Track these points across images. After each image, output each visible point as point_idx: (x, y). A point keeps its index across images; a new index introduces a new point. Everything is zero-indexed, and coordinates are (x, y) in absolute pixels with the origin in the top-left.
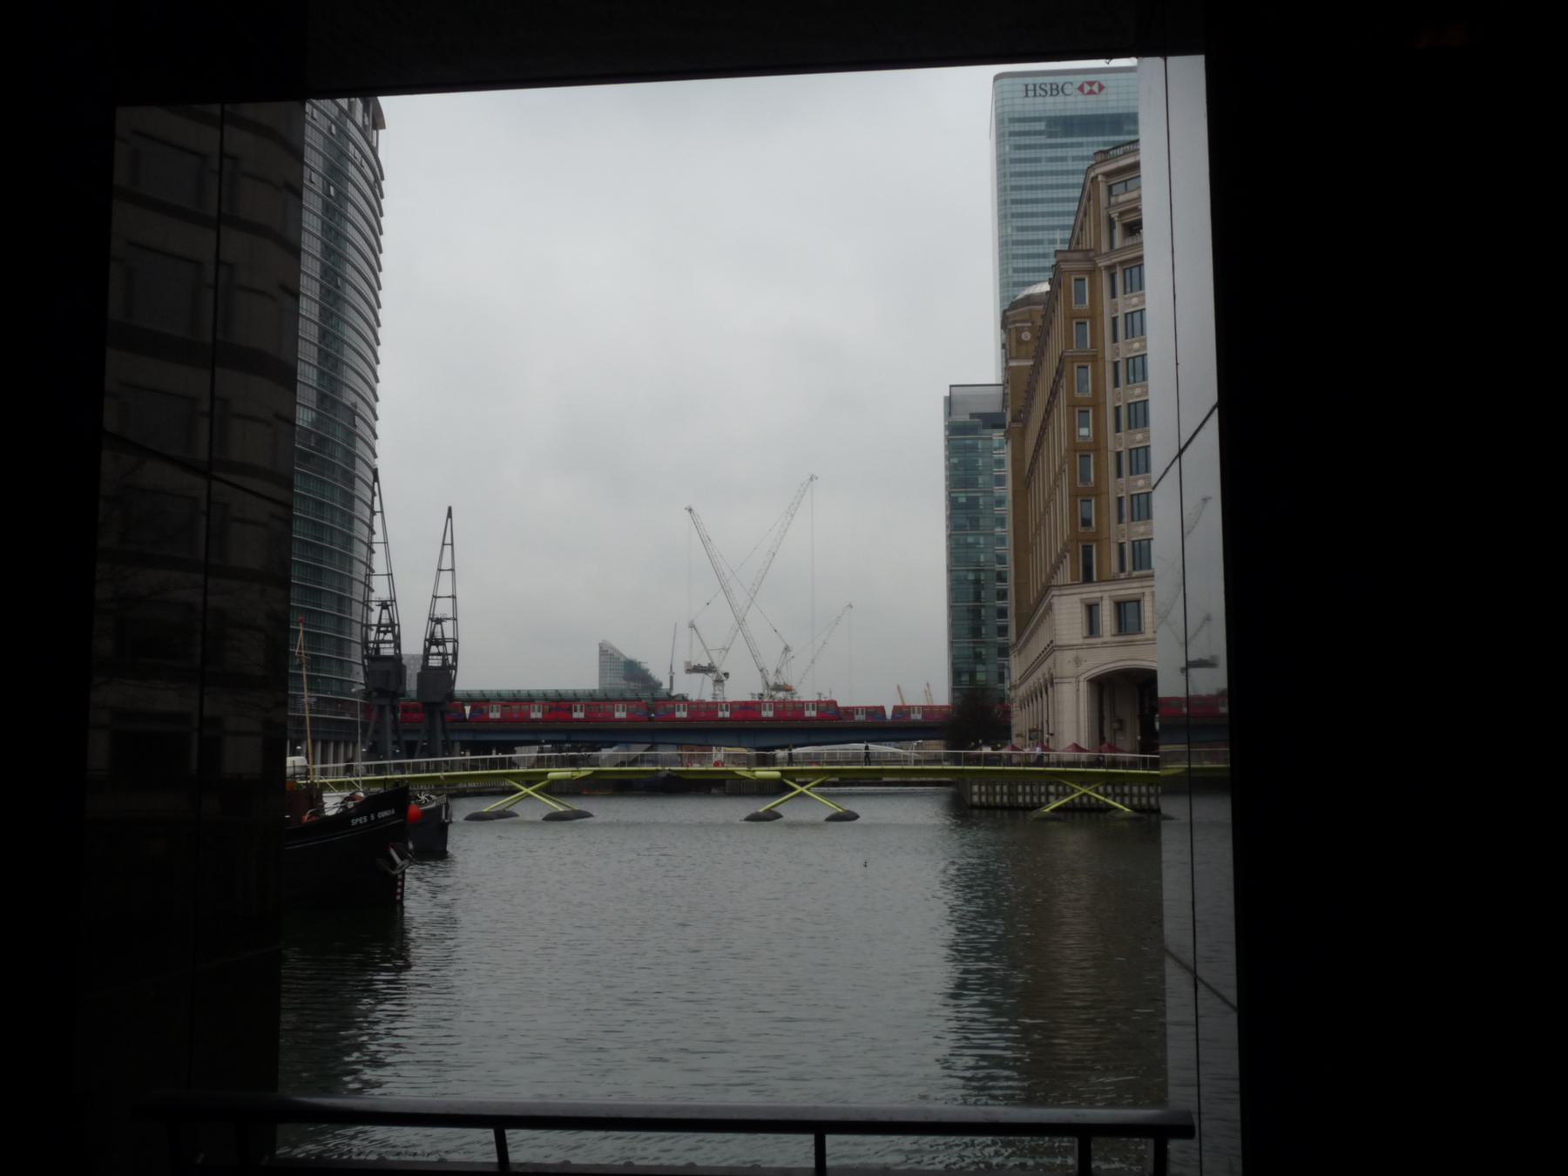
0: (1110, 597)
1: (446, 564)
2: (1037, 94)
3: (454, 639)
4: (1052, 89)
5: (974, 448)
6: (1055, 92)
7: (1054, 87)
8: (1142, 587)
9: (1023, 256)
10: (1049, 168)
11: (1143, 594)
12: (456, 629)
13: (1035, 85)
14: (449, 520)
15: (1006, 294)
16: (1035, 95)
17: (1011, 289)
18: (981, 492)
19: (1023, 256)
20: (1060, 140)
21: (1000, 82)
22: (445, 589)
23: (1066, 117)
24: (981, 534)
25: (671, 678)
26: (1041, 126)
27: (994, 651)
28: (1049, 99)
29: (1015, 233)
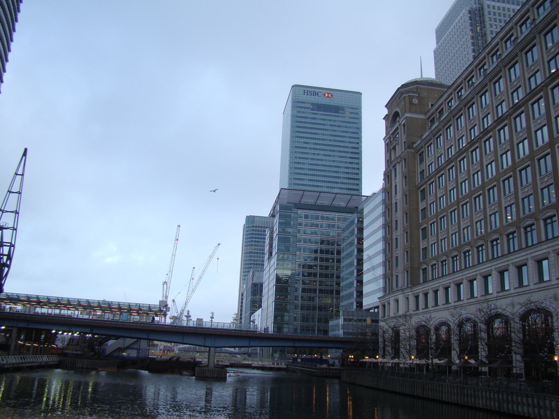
1: (20, 172)
2: (308, 94)
3: (11, 243)
5: (290, 217)
6: (315, 95)
7: (315, 93)
9: (299, 153)
12: (14, 236)
13: (307, 91)
14: (24, 157)
16: (307, 95)
18: (291, 235)
19: (299, 153)
20: (315, 112)
21: (294, 88)
22: (11, 206)
24: (290, 254)
25: (204, 271)
26: (309, 106)
27: (293, 307)
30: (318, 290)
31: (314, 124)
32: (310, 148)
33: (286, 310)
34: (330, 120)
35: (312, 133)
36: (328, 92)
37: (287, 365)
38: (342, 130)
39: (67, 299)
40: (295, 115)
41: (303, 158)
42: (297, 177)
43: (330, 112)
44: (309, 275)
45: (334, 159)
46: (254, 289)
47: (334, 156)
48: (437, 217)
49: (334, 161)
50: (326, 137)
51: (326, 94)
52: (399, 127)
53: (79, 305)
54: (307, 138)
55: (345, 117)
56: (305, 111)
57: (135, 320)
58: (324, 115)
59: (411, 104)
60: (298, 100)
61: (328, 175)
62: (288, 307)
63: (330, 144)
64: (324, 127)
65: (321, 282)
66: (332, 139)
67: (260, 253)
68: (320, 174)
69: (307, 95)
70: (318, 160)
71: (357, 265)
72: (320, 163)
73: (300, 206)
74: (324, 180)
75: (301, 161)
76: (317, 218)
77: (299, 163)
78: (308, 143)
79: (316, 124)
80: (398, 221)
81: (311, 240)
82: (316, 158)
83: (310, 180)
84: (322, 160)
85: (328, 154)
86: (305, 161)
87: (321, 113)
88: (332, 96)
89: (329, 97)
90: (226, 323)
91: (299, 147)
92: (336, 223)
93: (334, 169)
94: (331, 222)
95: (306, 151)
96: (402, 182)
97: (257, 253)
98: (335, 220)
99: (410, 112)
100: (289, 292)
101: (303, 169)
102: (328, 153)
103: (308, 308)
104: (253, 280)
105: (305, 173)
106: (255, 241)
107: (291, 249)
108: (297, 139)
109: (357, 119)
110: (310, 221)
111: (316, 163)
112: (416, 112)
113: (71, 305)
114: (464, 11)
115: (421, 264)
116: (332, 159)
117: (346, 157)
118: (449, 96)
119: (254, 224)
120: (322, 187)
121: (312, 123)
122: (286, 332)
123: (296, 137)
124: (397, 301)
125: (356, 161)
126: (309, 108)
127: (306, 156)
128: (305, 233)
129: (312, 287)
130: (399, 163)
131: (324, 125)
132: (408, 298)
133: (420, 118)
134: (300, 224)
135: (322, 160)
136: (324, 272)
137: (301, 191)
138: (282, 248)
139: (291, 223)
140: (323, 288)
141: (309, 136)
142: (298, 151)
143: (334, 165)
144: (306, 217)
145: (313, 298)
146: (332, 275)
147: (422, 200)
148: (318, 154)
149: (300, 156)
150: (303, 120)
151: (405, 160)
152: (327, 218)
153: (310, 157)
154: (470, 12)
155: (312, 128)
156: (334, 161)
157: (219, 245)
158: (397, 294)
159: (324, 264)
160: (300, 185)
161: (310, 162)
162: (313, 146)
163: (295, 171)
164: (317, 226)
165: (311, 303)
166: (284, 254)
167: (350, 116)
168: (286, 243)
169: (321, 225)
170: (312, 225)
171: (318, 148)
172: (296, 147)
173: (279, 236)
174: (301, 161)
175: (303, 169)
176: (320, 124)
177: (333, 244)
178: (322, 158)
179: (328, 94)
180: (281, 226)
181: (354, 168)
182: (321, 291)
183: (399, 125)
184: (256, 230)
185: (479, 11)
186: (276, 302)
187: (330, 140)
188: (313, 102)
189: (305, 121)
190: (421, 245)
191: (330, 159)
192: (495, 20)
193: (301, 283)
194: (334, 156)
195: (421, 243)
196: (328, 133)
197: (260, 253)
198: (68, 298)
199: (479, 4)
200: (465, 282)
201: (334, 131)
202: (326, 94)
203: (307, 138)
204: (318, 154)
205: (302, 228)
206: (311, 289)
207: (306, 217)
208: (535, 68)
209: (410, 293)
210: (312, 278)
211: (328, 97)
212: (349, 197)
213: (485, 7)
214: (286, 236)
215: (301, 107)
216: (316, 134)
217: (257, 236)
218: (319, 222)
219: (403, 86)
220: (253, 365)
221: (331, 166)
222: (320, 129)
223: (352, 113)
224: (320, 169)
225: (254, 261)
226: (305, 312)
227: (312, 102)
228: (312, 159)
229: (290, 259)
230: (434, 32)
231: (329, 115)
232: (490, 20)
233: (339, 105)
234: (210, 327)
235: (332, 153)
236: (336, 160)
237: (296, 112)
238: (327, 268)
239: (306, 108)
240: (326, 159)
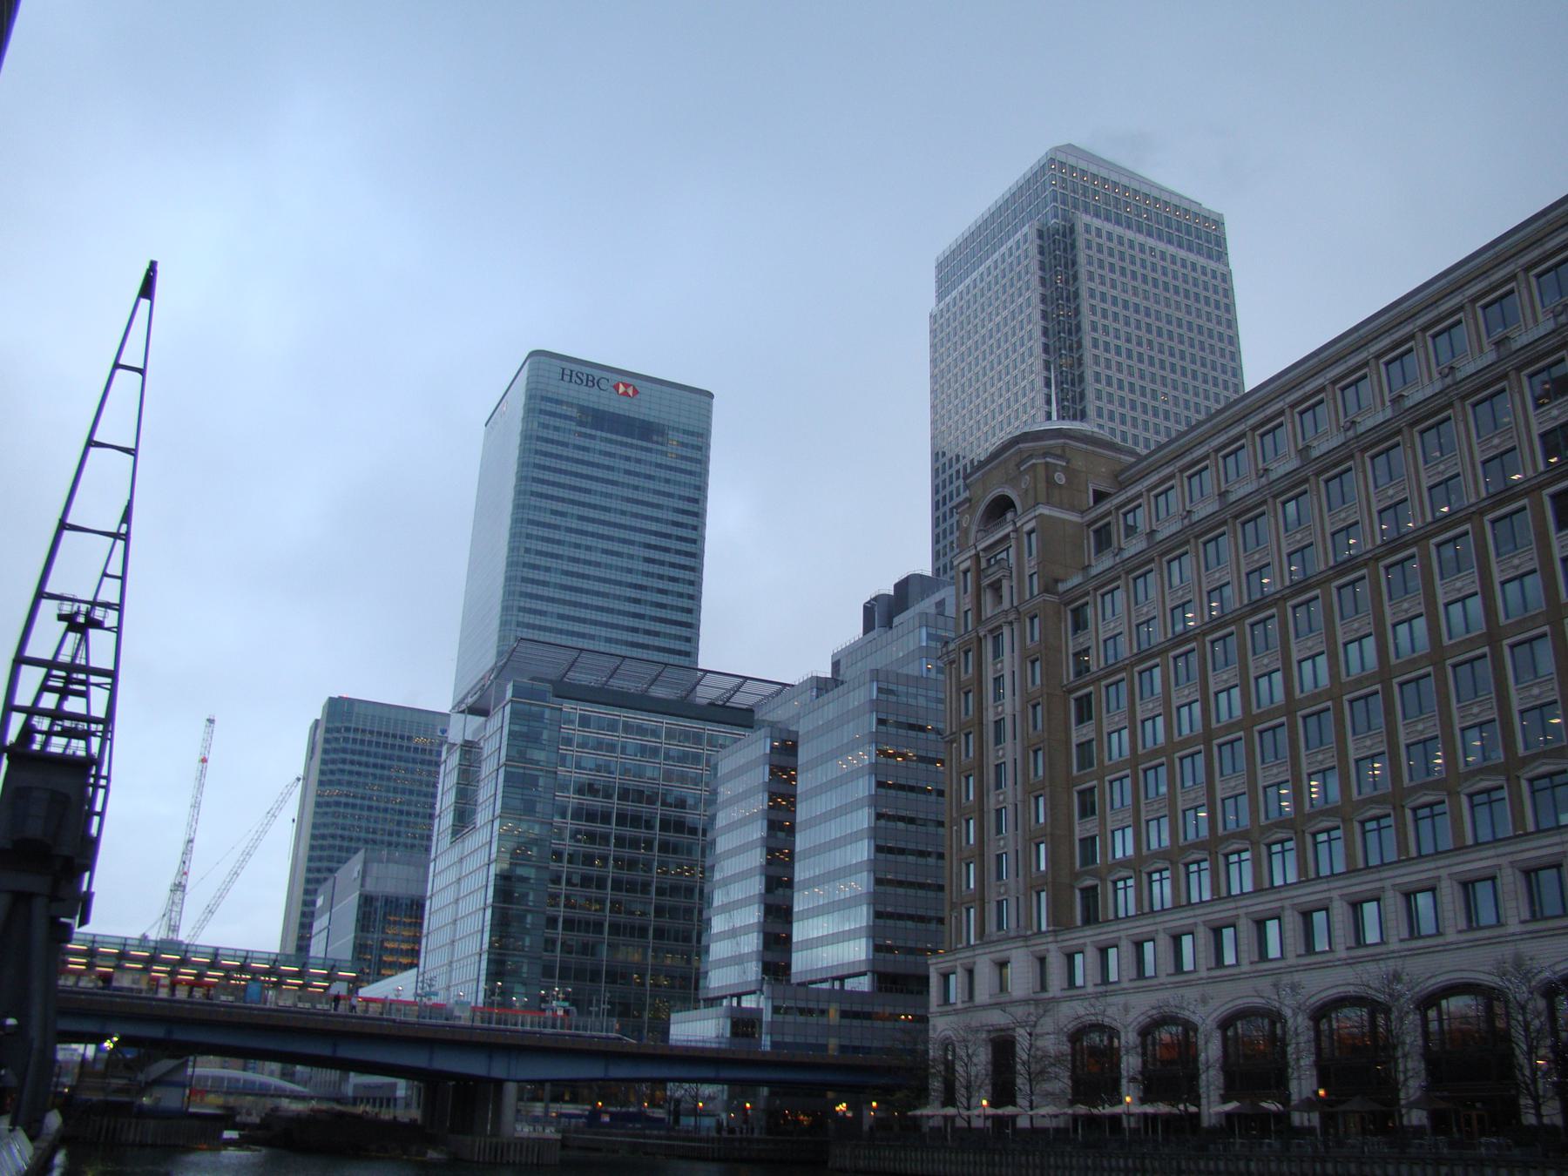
0: (1341, 896)
5: (541, 717)
6: (590, 384)
8: (1381, 880)
9: (539, 538)
11: (1331, 899)
19: (539, 538)
20: (588, 431)
21: (536, 359)
26: (574, 413)
30: (561, 920)
32: (569, 530)
34: (628, 459)
35: (574, 488)
36: (628, 380)
37: (564, 1131)
38: (657, 488)
41: (547, 554)
43: (1050, 517)
44: (586, 881)
46: (364, 913)
47: (631, 557)
49: (630, 571)
50: (614, 504)
51: (621, 386)
52: (1012, 535)
54: (563, 500)
55: (665, 454)
59: (1050, 482)
60: (544, 394)
67: (362, 807)
68: (590, 602)
70: (589, 563)
73: (565, 690)
75: (543, 561)
76: (612, 726)
77: (535, 567)
78: (563, 514)
83: (561, 617)
84: (598, 564)
85: (615, 549)
87: (604, 435)
88: (636, 392)
92: (663, 743)
94: (650, 742)
95: (557, 537)
97: (354, 806)
98: (659, 737)
101: (545, 584)
102: (616, 547)
104: (362, 885)
105: (551, 595)
106: (351, 773)
107: (539, 807)
108: (534, 501)
109: (699, 461)
110: (592, 734)
111: (581, 571)
112: (1061, 506)
114: (1026, 229)
115: (1076, 876)
116: (625, 565)
117: (662, 563)
118: (1162, 482)
119: (350, 721)
120: (592, 637)
121: (577, 461)
125: (687, 575)
126: (570, 418)
128: (578, 766)
132: (1042, 961)
134: (568, 741)
135: (598, 564)
136: (625, 875)
137: (568, 652)
140: (622, 918)
142: (535, 533)
144: (585, 721)
146: (645, 887)
147: (1080, 721)
148: (588, 548)
149: (539, 548)
152: (641, 730)
153: (566, 553)
154: (1040, 235)
155: (576, 475)
156: (630, 571)
158: (1004, 947)
159: (627, 853)
161: (565, 568)
162: (575, 524)
163: (524, 589)
164: (611, 747)
167: (679, 452)
170: (599, 745)
172: (531, 522)
174: (543, 561)
175: (545, 584)
176: (598, 466)
177: (651, 800)
179: (627, 386)
180: (516, 743)
181: (681, 595)
182: (615, 929)
184: (385, 746)
185: (1064, 236)
187: (623, 513)
188: (586, 404)
189: (559, 452)
190: (1077, 829)
191: (620, 564)
192: (1101, 265)
194: (631, 557)
197: (362, 807)
199: (1065, 219)
200: (959, 970)
201: (636, 488)
202: (621, 386)
203: (563, 500)
204: (588, 548)
205: (571, 752)
208: (1447, 469)
209: (1052, 947)
210: (593, 892)
211: (625, 394)
212: (659, 668)
213: (1080, 228)
216: (587, 491)
217: (356, 758)
218: (619, 737)
221: (619, 583)
222: (597, 479)
223: (683, 445)
224: (591, 587)
225: (343, 829)
230: (934, 265)
232: (1090, 263)
233: (652, 420)
235: (626, 549)
236: (635, 567)
237: (536, 425)
238: (632, 864)
239: (566, 417)
240: (609, 562)
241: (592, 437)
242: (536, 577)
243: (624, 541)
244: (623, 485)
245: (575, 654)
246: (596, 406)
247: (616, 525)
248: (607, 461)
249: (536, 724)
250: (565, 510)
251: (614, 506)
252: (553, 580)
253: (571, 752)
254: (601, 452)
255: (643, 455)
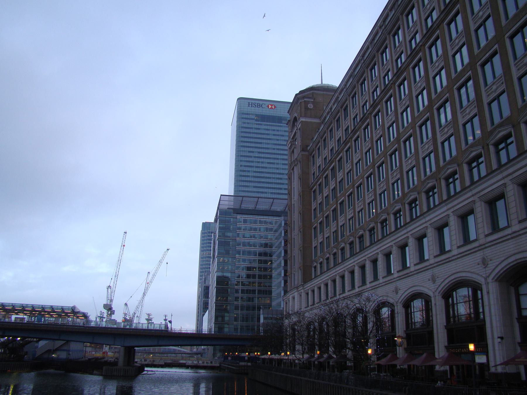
4: (258, 105)
6: (259, 106)
7: (259, 104)
9: (244, 161)
10: (255, 132)
13: (252, 103)
15: (236, 184)
16: (252, 106)
17: (240, 129)
18: (230, 239)
19: (244, 161)
20: (259, 123)
21: (239, 100)
23: (262, 115)
24: (230, 257)
26: (253, 117)
28: (257, 108)
29: (243, 124)
30: (257, 291)
31: (258, 133)
33: (226, 310)
34: (274, 130)
36: (272, 103)
39: (61, 307)
40: (241, 126)
42: (242, 184)
45: (277, 167)
47: (278, 164)
48: (323, 216)
49: (278, 169)
51: (270, 105)
53: (23, 309)
56: (250, 122)
57: (49, 322)
58: (268, 125)
59: (307, 109)
60: (243, 112)
61: (272, 181)
62: (228, 308)
63: (274, 152)
64: (268, 137)
65: (260, 283)
66: (276, 147)
68: (264, 181)
69: (252, 106)
70: (263, 167)
71: (284, 266)
72: (264, 171)
74: (268, 186)
75: (247, 169)
78: (253, 152)
79: (260, 134)
80: (295, 221)
81: (250, 243)
82: (260, 166)
83: (255, 187)
85: (272, 162)
86: (249, 169)
87: (265, 123)
88: (275, 107)
89: (273, 109)
90: (156, 324)
91: (244, 156)
93: (278, 176)
95: (251, 160)
96: (298, 182)
98: (272, 224)
99: (305, 116)
100: (229, 293)
101: (248, 176)
102: (272, 161)
103: (248, 308)
105: (250, 180)
107: (231, 252)
108: (242, 149)
110: (248, 225)
112: (311, 117)
113: (54, 312)
116: (276, 167)
120: (266, 193)
121: (256, 133)
122: (226, 332)
123: (242, 146)
124: (294, 298)
126: (253, 119)
127: (251, 164)
128: (244, 237)
129: (251, 288)
130: (296, 165)
131: (268, 134)
132: (301, 296)
133: (315, 122)
134: (240, 229)
136: (263, 273)
137: (240, 197)
138: (223, 251)
139: (230, 227)
140: (262, 288)
141: (253, 145)
143: (277, 172)
144: (245, 221)
145: (253, 298)
148: (262, 162)
149: (245, 164)
150: (248, 130)
151: (300, 162)
152: (266, 223)
153: (255, 165)
155: (256, 138)
156: (278, 169)
157: (168, 250)
158: (294, 292)
159: (263, 265)
160: (245, 191)
161: (255, 170)
164: (255, 229)
165: (250, 303)
166: (224, 257)
168: (225, 247)
169: (259, 229)
170: (251, 229)
171: (262, 156)
172: (242, 156)
173: (219, 240)
174: (247, 169)
175: (248, 176)
176: (264, 134)
178: (266, 166)
179: (272, 105)
182: (260, 292)
183: (297, 129)
186: (217, 303)
187: (274, 149)
188: (258, 113)
190: (313, 243)
191: (274, 167)
193: (240, 285)
194: (278, 164)
195: (313, 242)
196: (272, 142)
198: (62, 307)
201: (278, 140)
202: (270, 105)
204: (262, 162)
205: (241, 232)
206: (266, 291)
207: (245, 221)
209: (302, 291)
210: (251, 280)
211: (271, 108)
214: (225, 240)
215: (246, 118)
216: (261, 143)
218: (258, 226)
219: (301, 92)
220: (187, 364)
222: (264, 139)
226: (245, 312)
227: (256, 113)
228: (257, 167)
229: (230, 262)
231: (273, 126)
233: (282, 116)
234: (146, 328)
235: (276, 161)
237: (241, 123)
239: (251, 119)
241: (261, 124)
242: (245, 174)
243: (275, 159)
244: (273, 139)
245: (272, 200)
246: (261, 114)
247: (271, 154)
248: (267, 132)
249: (228, 224)
250: (253, 150)
251: (270, 147)
252: (251, 175)
253: (241, 232)
254: (264, 129)
255: (279, 128)
